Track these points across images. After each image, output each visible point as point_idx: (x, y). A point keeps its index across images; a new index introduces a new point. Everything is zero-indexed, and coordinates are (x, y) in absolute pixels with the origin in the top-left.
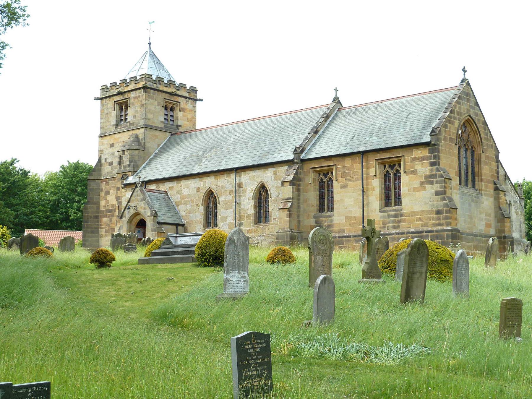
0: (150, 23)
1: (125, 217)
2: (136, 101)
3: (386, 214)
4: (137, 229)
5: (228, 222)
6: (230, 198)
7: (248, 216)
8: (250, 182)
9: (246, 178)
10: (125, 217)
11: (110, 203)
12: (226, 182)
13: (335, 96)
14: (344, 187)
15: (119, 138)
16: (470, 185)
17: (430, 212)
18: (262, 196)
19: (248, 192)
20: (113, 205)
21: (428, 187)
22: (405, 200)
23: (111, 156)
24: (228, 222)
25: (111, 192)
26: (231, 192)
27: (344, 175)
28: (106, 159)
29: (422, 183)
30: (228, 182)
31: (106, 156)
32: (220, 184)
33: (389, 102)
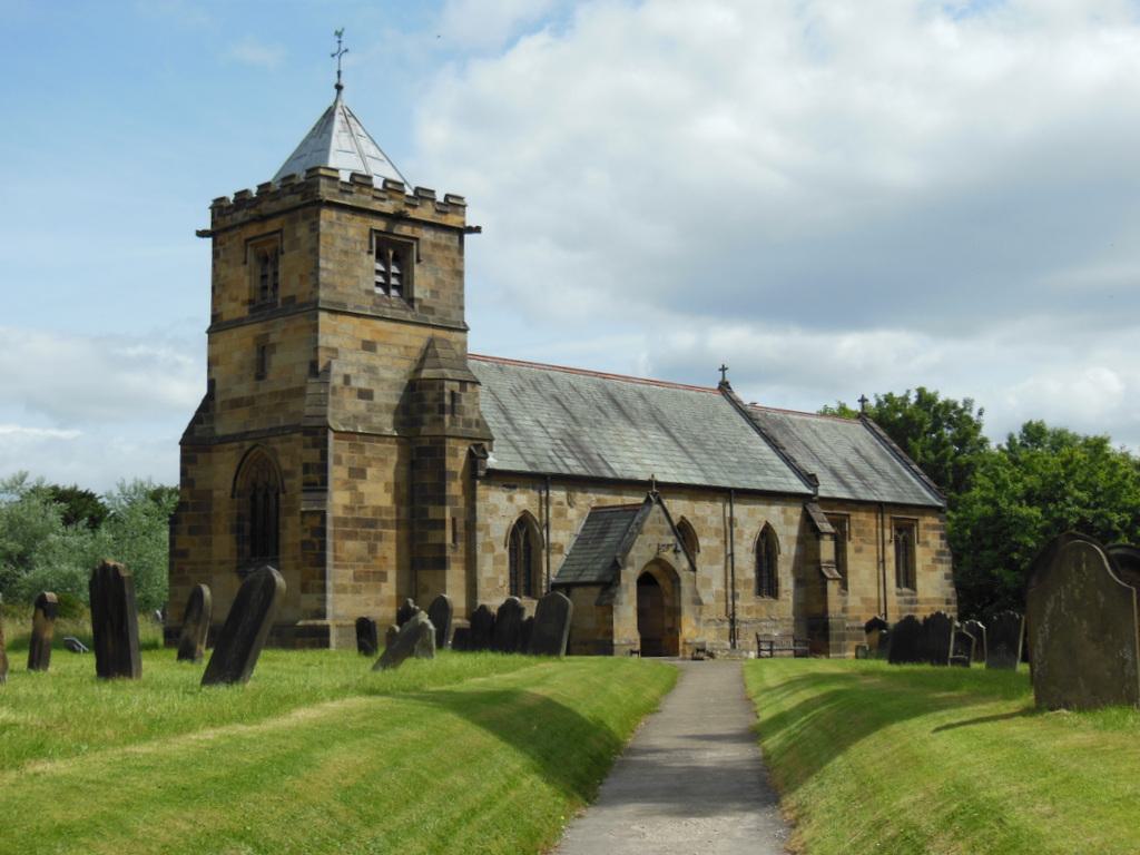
0: (339, 34)
1: (632, 565)
2: (438, 254)
3: (903, 598)
4: (71, 529)
5: (714, 588)
6: (716, 542)
7: (746, 582)
8: (750, 519)
9: (740, 510)
10: (632, 565)
11: (370, 502)
12: (708, 511)
13: (720, 379)
14: (858, 550)
15: (391, 333)
16: (305, 488)
17: (941, 600)
18: (766, 544)
19: (745, 537)
20: (377, 510)
21: (939, 566)
22: (920, 583)
23: (366, 375)
24: (714, 588)
25: (370, 472)
26: (717, 532)
27: (859, 532)
28: (347, 379)
29: (934, 561)
30: (713, 512)
31: (348, 370)
32: (699, 513)
33: (796, 417)
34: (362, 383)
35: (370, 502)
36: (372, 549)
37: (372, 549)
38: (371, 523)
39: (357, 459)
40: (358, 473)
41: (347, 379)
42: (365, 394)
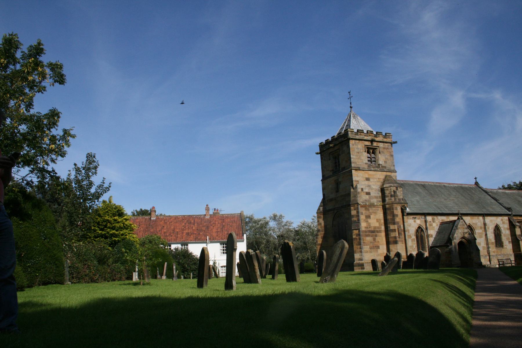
7: (492, 243)
9: (488, 219)
18: (497, 229)
20: (375, 227)
28: (362, 189)
34: (366, 190)
35: (372, 225)
36: (374, 239)
37: (374, 239)
38: (373, 232)
39: (368, 213)
40: (368, 217)
41: (362, 189)
42: (368, 194)
